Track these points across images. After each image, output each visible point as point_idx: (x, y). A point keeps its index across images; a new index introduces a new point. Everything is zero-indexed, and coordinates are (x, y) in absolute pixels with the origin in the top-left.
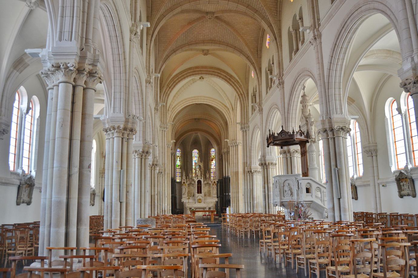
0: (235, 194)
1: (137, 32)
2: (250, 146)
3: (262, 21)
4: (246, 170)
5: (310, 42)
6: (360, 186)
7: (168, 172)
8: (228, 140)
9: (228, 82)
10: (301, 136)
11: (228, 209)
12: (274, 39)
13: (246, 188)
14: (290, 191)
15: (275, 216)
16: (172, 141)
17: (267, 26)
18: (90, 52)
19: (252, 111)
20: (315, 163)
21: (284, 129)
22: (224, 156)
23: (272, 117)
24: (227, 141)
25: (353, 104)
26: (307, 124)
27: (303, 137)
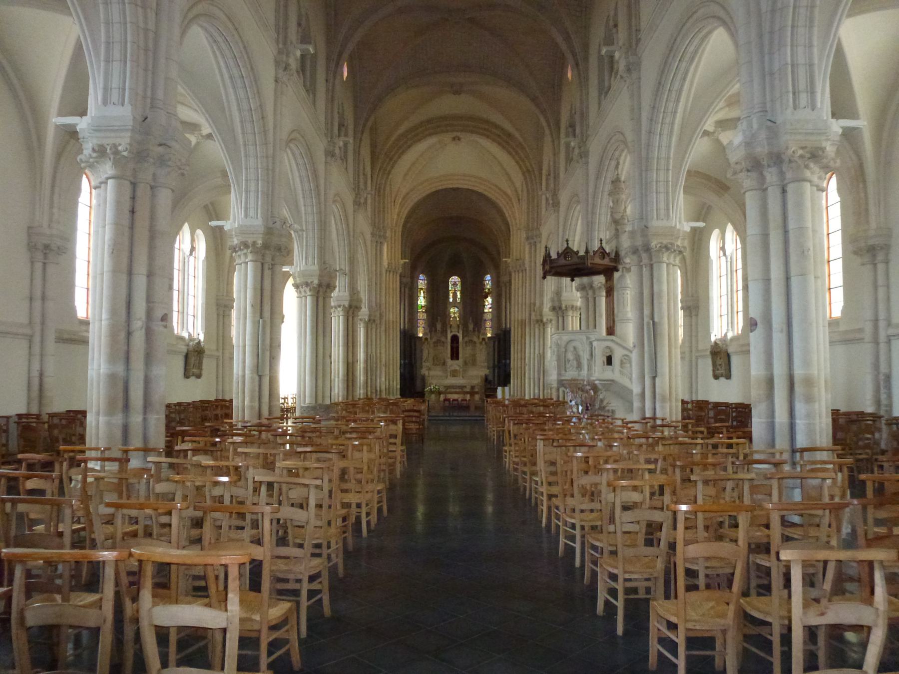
4: (533, 317)
6: (736, 353)
8: (509, 260)
9: (504, 147)
16: (402, 262)
21: (570, 245)
22: (503, 288)
27: (606, 262)
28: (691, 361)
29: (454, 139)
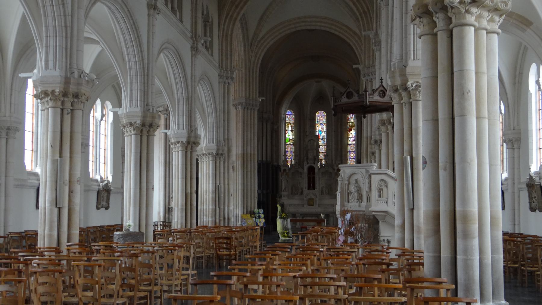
7: (252, 153)
25: (528, 30)
28: (514, 193)
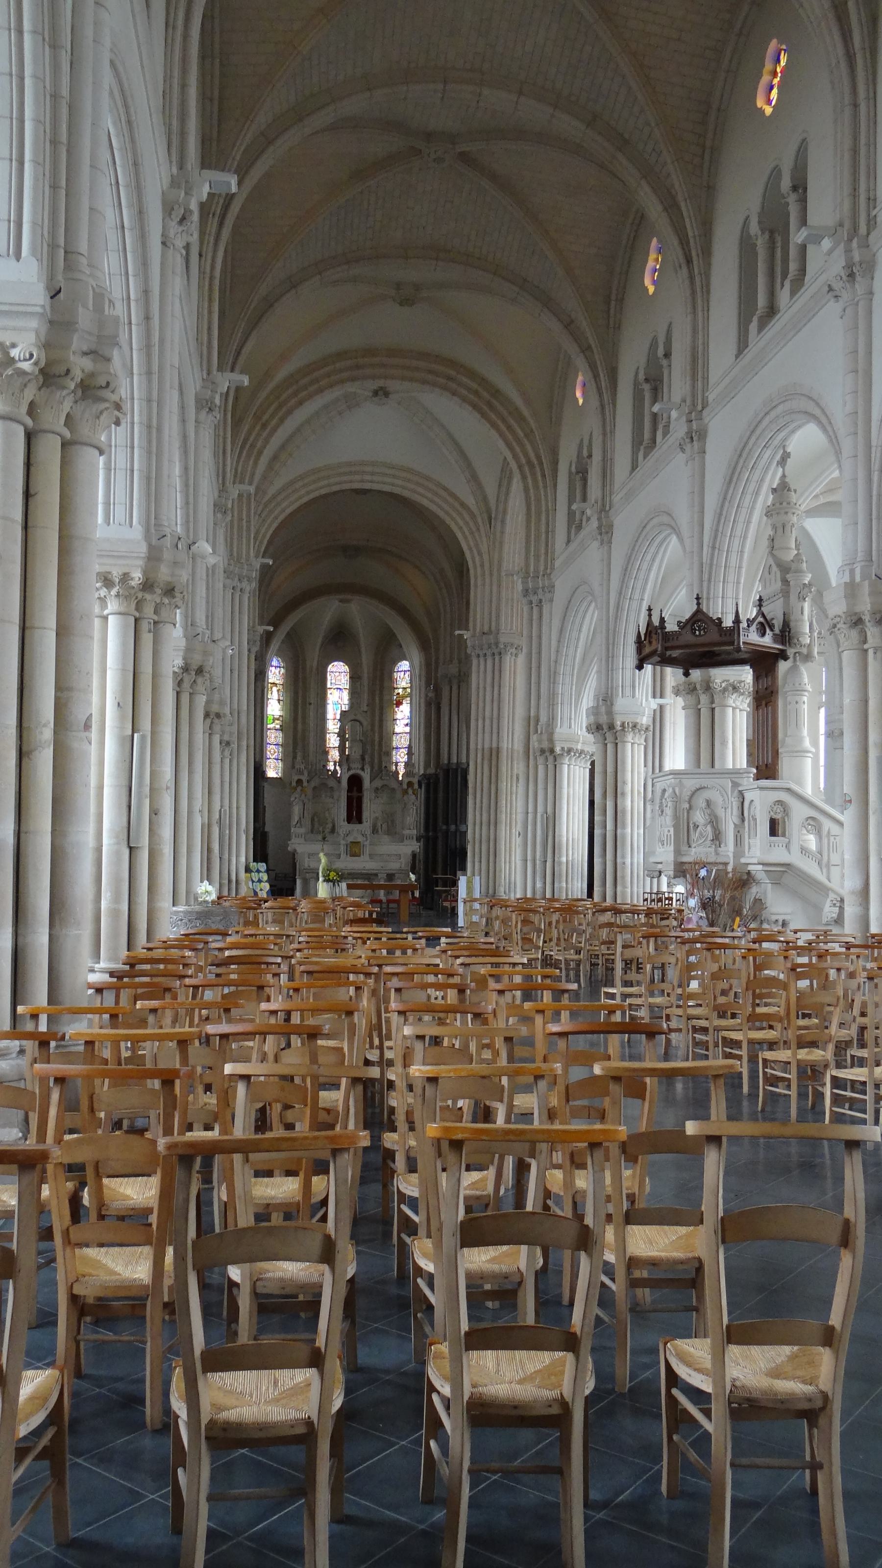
0: (484, 828)
1: (191, 212)
2: (553, 658)
3: (643, 182)
5: (831, 289)
8: (466, 635)
10: (763, 634)
11: (462, 882)
12: (682, 260)
13: (530, 810)
14: (713, 826)
15: (634, 911)
17: (660, 208)
18: (85, 306)
19: (569, 533)
20: (805, 732)
23: (649, 557)
24: (461, 636)
26: (785, 592)
27: (767, 641)
29: (376, 393)
